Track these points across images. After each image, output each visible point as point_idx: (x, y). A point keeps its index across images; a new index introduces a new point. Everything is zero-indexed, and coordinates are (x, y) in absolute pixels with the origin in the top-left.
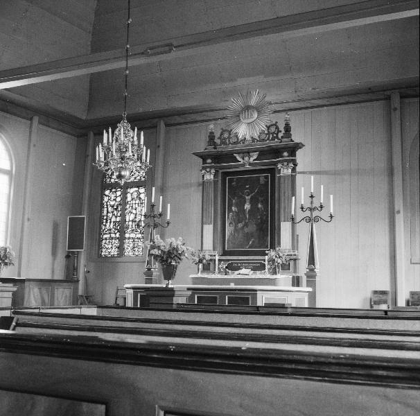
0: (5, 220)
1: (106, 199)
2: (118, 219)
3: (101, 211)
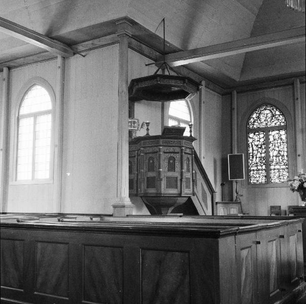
1: (250, 140)
2: (263, 155)
3: (248, 150)
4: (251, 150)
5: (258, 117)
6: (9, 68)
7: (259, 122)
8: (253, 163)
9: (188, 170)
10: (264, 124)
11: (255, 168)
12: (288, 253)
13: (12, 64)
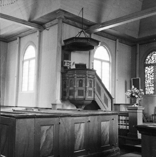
0: (109, 81)
1: (146, 71)
2: (153, 79)
3: (144, 76)
4: (146, 76)
5: (150, 58)
6: (20, 38)
7: (151, 60)
8: (147, 83)
9: (91, 86)
10: (153, 61)
11: (149, 86)
12: (104, 130)
13: (20, 36)
